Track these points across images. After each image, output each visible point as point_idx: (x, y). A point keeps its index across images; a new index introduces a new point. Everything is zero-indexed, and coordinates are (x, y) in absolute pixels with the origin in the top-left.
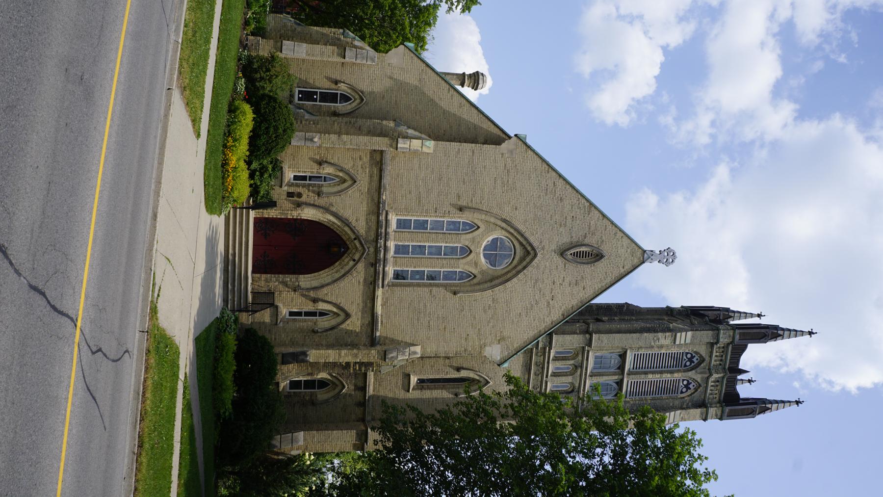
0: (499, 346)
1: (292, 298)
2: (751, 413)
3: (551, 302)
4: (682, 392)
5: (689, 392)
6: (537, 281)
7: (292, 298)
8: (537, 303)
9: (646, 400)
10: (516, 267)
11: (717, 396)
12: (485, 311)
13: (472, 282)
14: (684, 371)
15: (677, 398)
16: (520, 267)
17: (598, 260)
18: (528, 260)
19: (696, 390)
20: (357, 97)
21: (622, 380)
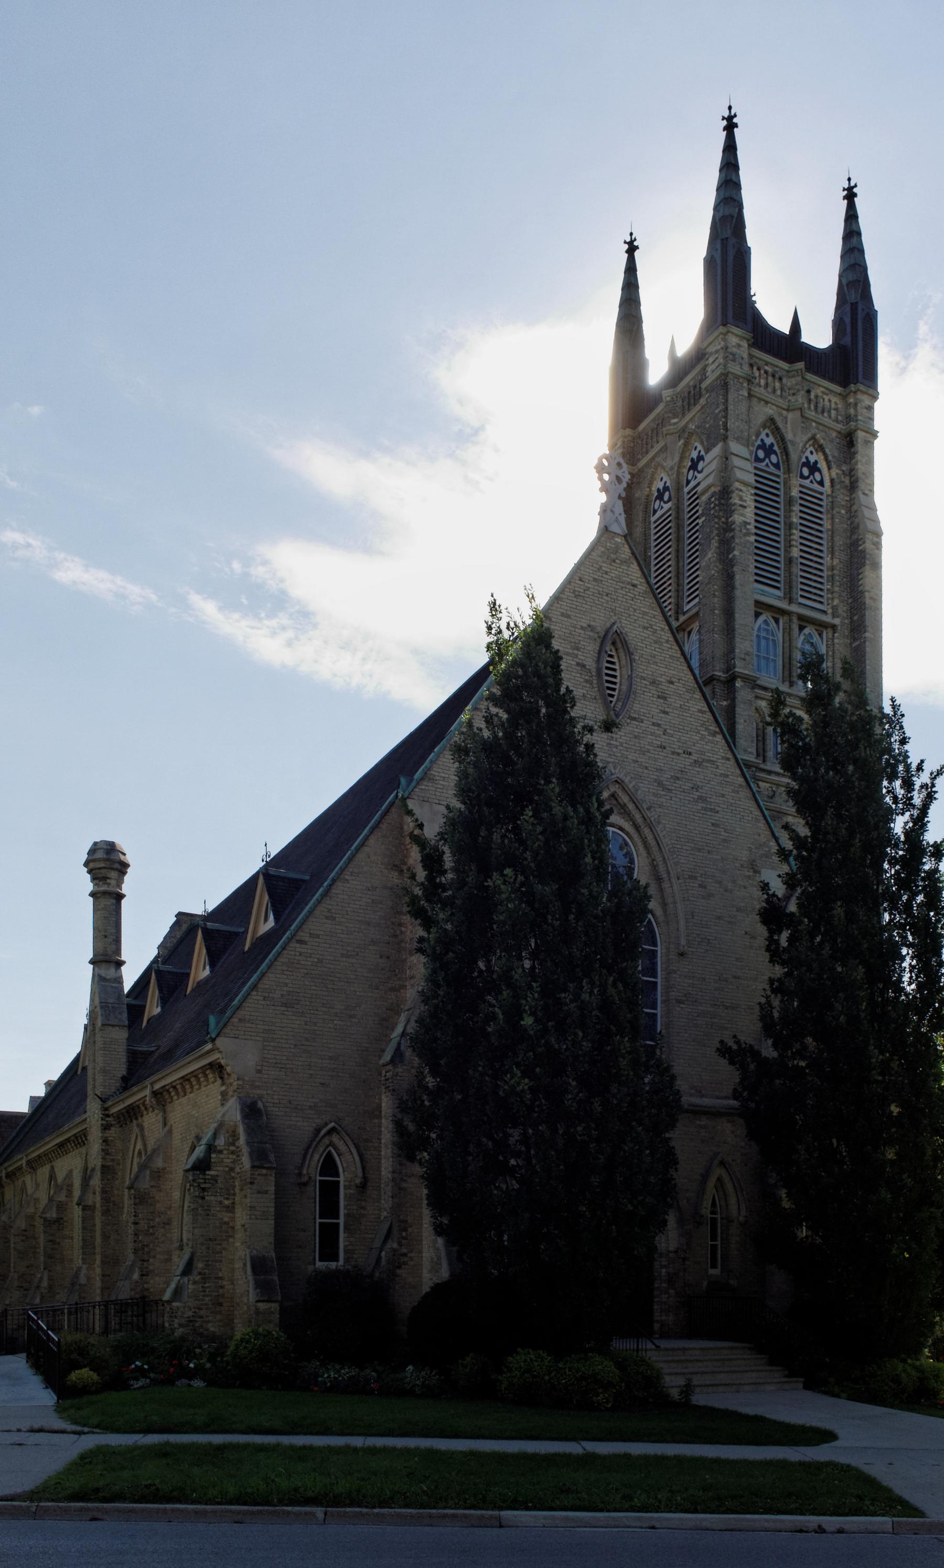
0: (763, 871)
1: (266, 1192)
2: (870, 319)
3: (694, 757)
4: (821, 483)
5: (822, 465)
6: (660, 784)
7: (266, 1192)
8: (696, 788)
9: (832, 568)
10: (637, 827)
11: (834, 399)
12: (710, 896)
13: (661, 919)
14: (788, 471)
15: (832, 496)
16: (638, 817)
17: (625, 644)
18: (624, 799)
19: (820, 448)
20: (326, 1141)
21: (801, 618)
